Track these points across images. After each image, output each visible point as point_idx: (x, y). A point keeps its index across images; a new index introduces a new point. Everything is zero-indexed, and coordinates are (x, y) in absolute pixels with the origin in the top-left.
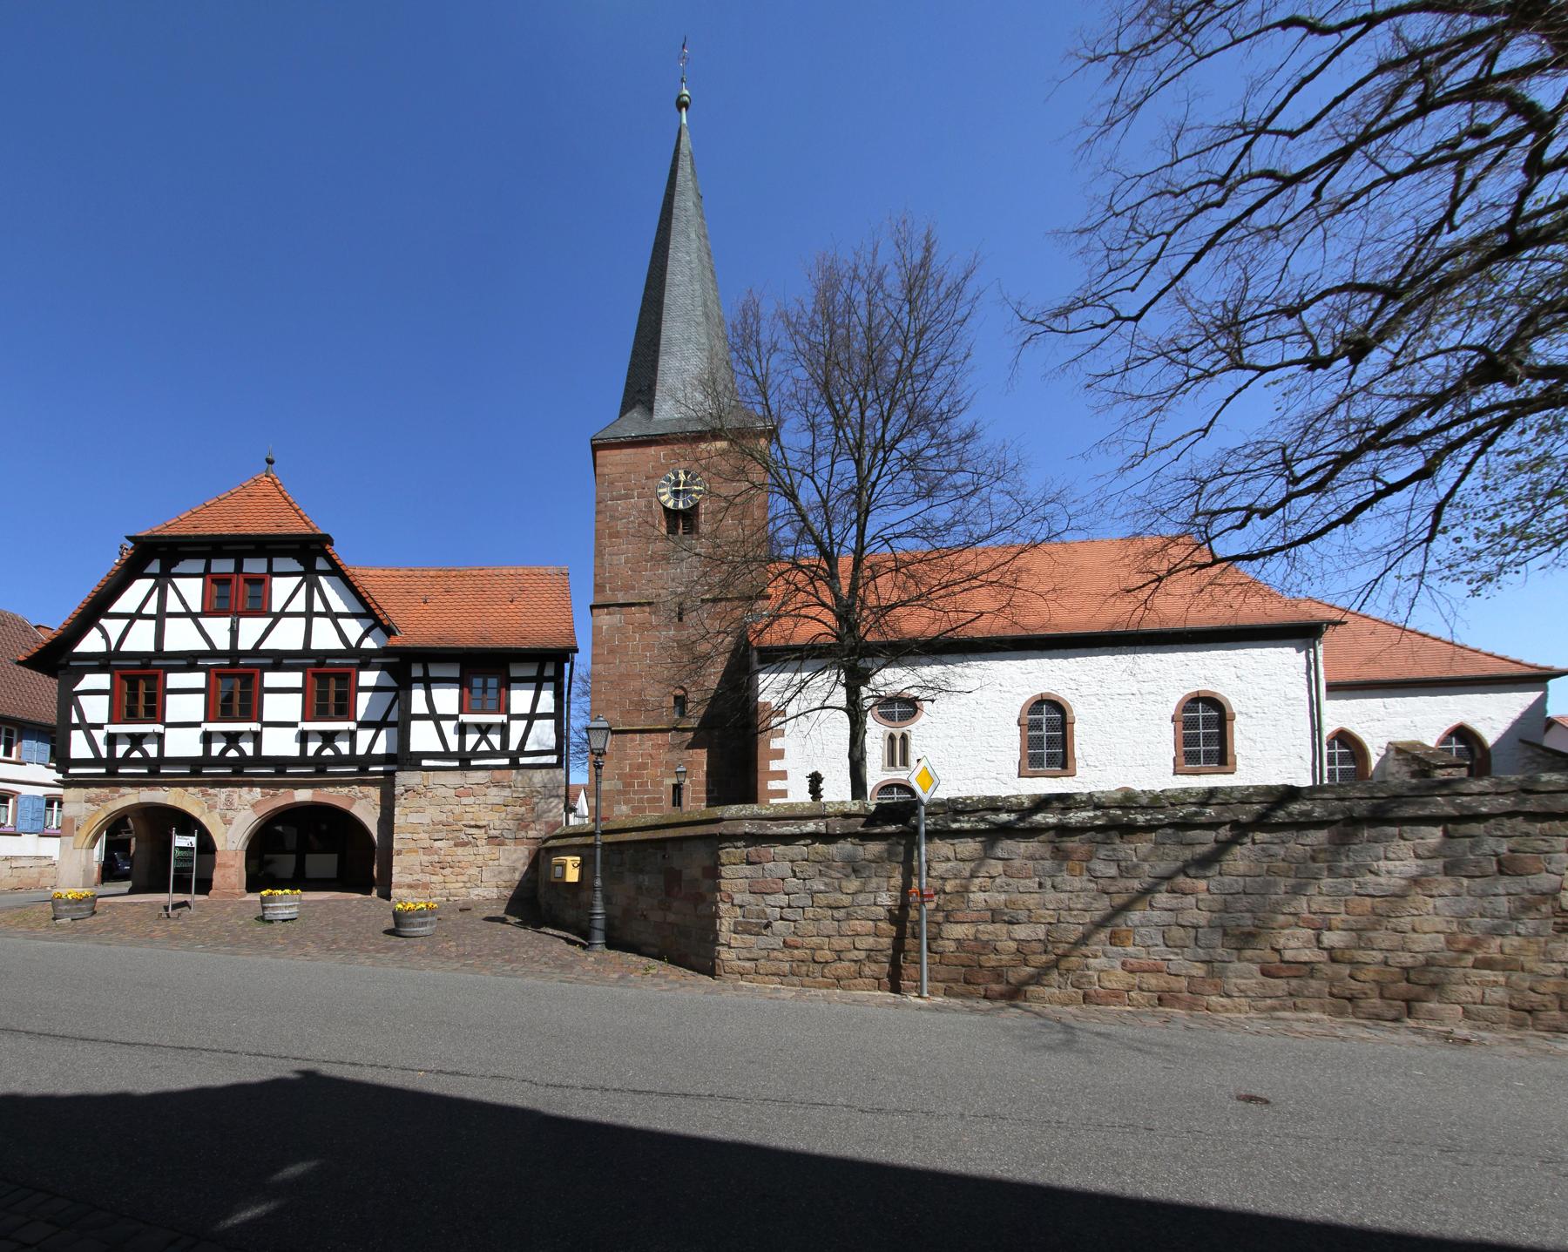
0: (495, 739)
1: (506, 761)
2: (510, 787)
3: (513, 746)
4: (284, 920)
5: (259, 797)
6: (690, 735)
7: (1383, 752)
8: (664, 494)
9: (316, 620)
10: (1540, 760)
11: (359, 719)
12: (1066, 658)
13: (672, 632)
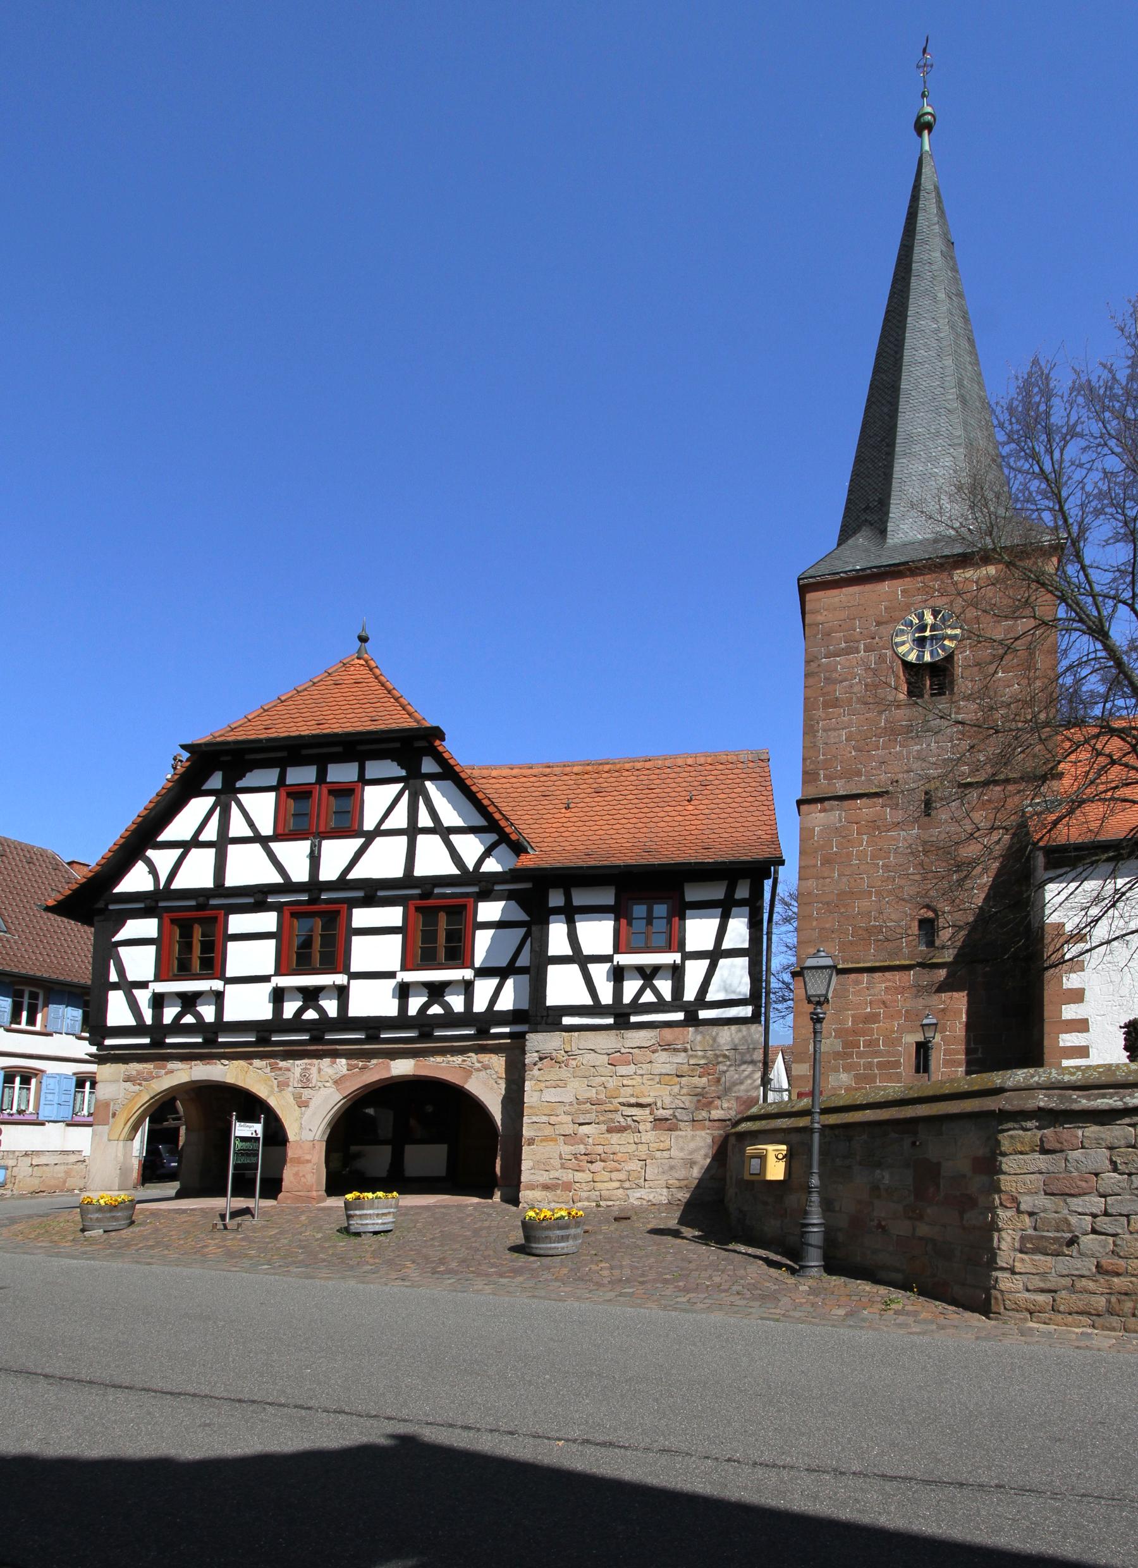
0: (665, 987)
1: (679, 1016)
2: (685, 1050)
3: (690, 995)
4: (376, 1233)
5: (345, 1071)
6: (943, 973)
8: (903, 643)
9: (421, 839)
11: (477, 964)
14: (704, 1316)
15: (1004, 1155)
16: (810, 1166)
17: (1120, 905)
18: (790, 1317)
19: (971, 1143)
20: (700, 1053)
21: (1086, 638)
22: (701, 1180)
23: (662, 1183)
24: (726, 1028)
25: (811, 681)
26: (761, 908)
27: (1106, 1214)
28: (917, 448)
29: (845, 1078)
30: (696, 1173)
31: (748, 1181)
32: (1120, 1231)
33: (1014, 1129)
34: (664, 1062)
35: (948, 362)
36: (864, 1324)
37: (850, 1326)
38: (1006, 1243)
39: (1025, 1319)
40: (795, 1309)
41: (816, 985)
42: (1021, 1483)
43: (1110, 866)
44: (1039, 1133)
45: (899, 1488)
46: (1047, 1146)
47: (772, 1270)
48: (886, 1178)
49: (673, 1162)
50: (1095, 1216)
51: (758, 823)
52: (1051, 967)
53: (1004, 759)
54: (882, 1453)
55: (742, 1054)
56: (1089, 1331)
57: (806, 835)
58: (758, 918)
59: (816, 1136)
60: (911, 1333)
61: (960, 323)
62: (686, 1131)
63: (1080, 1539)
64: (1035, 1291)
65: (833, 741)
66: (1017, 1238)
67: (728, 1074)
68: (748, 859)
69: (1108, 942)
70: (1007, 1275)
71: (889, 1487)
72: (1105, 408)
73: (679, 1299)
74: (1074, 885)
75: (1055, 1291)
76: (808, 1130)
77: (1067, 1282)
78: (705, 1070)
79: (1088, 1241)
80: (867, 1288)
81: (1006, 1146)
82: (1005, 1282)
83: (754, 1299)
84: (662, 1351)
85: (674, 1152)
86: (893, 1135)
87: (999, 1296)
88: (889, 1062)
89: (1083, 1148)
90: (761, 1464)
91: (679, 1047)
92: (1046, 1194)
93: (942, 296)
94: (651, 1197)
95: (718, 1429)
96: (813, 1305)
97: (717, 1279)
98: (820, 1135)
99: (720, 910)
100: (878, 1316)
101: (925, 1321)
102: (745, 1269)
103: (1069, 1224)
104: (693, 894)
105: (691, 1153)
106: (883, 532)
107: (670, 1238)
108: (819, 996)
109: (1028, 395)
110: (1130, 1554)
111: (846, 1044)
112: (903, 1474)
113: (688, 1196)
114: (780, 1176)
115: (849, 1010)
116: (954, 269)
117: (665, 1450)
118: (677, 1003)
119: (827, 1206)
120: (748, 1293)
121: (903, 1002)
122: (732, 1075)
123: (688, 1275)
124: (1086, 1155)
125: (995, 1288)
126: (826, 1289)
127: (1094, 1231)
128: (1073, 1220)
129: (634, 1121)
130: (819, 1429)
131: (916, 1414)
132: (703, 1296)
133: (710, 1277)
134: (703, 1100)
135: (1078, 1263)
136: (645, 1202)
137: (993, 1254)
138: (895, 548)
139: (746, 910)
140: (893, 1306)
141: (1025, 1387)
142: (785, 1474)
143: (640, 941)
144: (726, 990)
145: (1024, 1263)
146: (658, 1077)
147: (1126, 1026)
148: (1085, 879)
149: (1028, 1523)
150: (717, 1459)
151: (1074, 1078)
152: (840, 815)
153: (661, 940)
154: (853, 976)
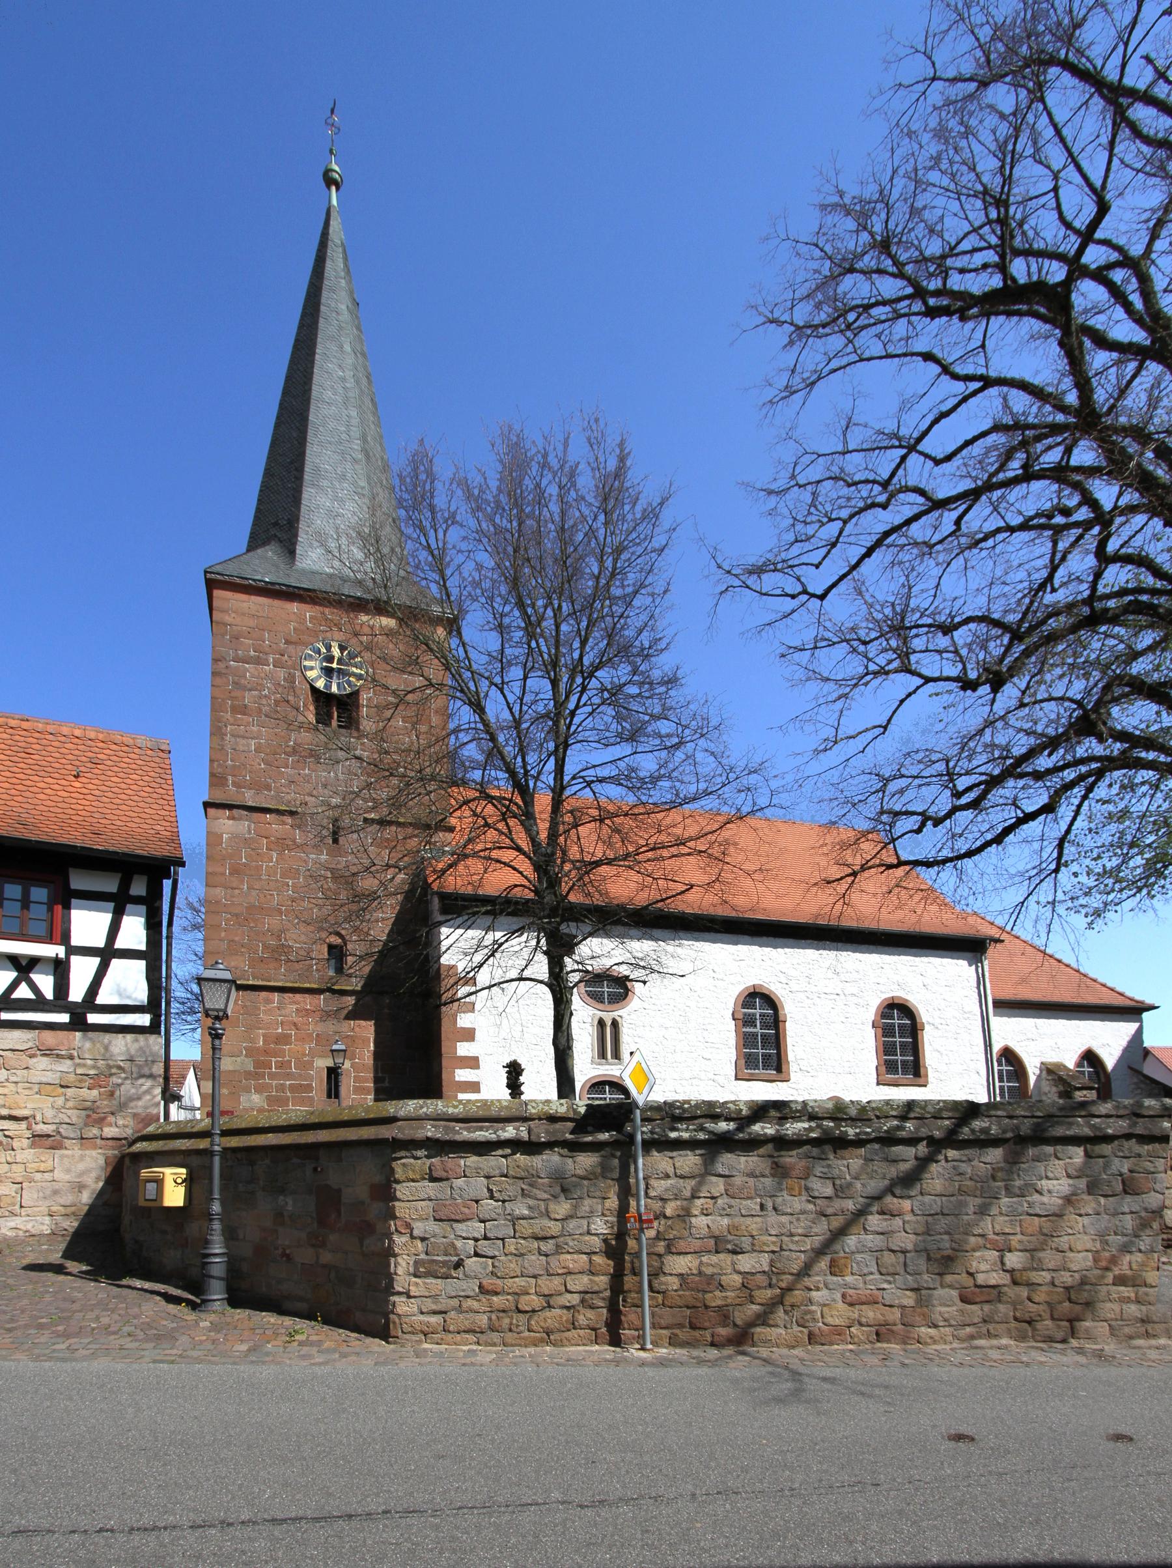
0: (46, 983)
1: (64, 1018)
2: (71, 1058)
3: (77, 993)
6: (351, 1000)
7: (1038, 1072)
8: (312, 668)
10: (1142, 1086)
12: (775, 947)
13: (324, 857)
14: (85, 1364)
15: (398, 1182)
16: (211, 1192)
17: (497, 955)
18: (188, 1357)
19: (366, 1171)
20: (89, 1062)
21: (467, 708)
22: (92, 1207)
23: (44, 1209)
24: (120, 1036)
25: (218, 681)
26: (160, 909)
27: (486, 1238)
28: (325, 483)
29: (256, 1099)
30: (86, 1198)
31: (144, 1208)
32: (497, 1253)
33: (406, 1157)
34: (43, 1069)
35: (354, 413)
36: (267, 1359)
37: (252, 1362)
38: (402, 1266)
39: (420, 1341)
40: (194, 1349)
41: (215, 999)
42: (405, 1506)
43: (488, 920)
44: (428, 1162)
45: (288, 1531)
46: (435, 1175)
47: (171, 1306)
48: (289, 1204)
49: (56, 1186)
50: (476, 1240)
51: (157, 817)
52: (445, 1004)
53: (395, 803)
54: (274, 1496)
55: (140, 1067)
56: (475, 1347)
57: (213, 839)
58: (157, 920)
59: (217, 1160)
60: (314, 1364)
61: (364, 381)
62: (73, 1151)
63: (454, 1551)
64: (428, 1313)
65: (241, 748)
66: (411, 1263)
67: (123, 1087)
68: (145, 853)
69: (489, 987)
70: (404, 1299)
71: (277, 1531)
72: (479, 508)
73: (57, 1347)
74: (460, 931)
75: (445, 1313)
76: (208, 1153)
77: (455, 1303)
78: (96, 1081)
79: (472, 1263)
80: (272, 1320)
81: (399, 1174)
82: (402, 1306)
83: (147, 1339)
84: (28, 1410)
85: (58, 1174)
86: (295, 1160)
87: (397, 1320)
88: (301, 1085)
89: (465, 1176)
90: (138, 1529)
91: (63, 1053)
92: (435, 1220)
93: (347, 348)
94: (29, 1226)
95: (90, 1495)
96: (214, 1342)
97: (105, 1320)
98: (222, 1158)
99: (112, 905)
100: (281, 1349)
101: (328, 1351)
102: (140, 1306)
103: (455, 1248)
104: (79, 881)
105: (82, 1174)
106: (292, 553)
107: (50, 1274)
108: (218, 1010)
109: (415, 469)
110: (495, 1557)
111: (258, 1064)
112: (293, 1515)
113: (76, 1224)
114: (180, 1202)
115: (260, 1028)
116: (358, 328)
117: (20, 1532)
118: (60, 1002)
119: (230, 1234)
120: (141, 1335)
121: (314, 1026)
122: (128, 1089)
123: (70, 1318)
124: (468, 1185)
125: (393, 1312)
126: (228, 1324)
127: (476, 1254)
128: (459, 1244)
129: (6, 1136)
130: (208, 1480)
131: (312, 1449)
132: (86, 1341)
133: (97, 1318)
134: (93, 1115)
135: (464, 1284)
136: (21, 1233)
137: (390, 1278)
138: (304, 572)
139: (143, 909)
140: (297, 1337)
141: (416, 1408)
142: (166, 1537)
143: (41, 929)
144: (120, 994)
145: (418, 1286)
146: (37, 1086)
147: (508, 1066)
148: (469, 928)
149: (409, 1545)
150: (85, 1531)
151: (456, 1111)
152: (249, 827)
153: (41, 929)
154: (264, 994)
